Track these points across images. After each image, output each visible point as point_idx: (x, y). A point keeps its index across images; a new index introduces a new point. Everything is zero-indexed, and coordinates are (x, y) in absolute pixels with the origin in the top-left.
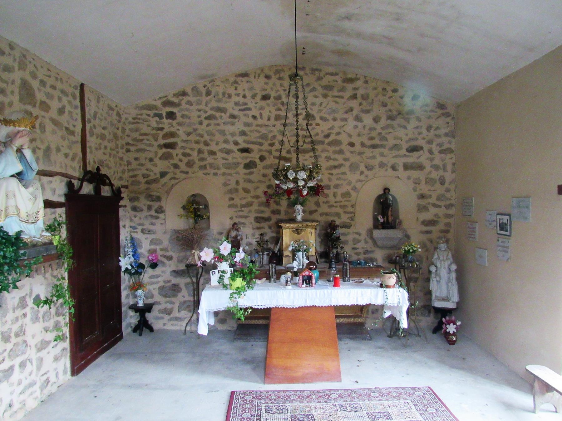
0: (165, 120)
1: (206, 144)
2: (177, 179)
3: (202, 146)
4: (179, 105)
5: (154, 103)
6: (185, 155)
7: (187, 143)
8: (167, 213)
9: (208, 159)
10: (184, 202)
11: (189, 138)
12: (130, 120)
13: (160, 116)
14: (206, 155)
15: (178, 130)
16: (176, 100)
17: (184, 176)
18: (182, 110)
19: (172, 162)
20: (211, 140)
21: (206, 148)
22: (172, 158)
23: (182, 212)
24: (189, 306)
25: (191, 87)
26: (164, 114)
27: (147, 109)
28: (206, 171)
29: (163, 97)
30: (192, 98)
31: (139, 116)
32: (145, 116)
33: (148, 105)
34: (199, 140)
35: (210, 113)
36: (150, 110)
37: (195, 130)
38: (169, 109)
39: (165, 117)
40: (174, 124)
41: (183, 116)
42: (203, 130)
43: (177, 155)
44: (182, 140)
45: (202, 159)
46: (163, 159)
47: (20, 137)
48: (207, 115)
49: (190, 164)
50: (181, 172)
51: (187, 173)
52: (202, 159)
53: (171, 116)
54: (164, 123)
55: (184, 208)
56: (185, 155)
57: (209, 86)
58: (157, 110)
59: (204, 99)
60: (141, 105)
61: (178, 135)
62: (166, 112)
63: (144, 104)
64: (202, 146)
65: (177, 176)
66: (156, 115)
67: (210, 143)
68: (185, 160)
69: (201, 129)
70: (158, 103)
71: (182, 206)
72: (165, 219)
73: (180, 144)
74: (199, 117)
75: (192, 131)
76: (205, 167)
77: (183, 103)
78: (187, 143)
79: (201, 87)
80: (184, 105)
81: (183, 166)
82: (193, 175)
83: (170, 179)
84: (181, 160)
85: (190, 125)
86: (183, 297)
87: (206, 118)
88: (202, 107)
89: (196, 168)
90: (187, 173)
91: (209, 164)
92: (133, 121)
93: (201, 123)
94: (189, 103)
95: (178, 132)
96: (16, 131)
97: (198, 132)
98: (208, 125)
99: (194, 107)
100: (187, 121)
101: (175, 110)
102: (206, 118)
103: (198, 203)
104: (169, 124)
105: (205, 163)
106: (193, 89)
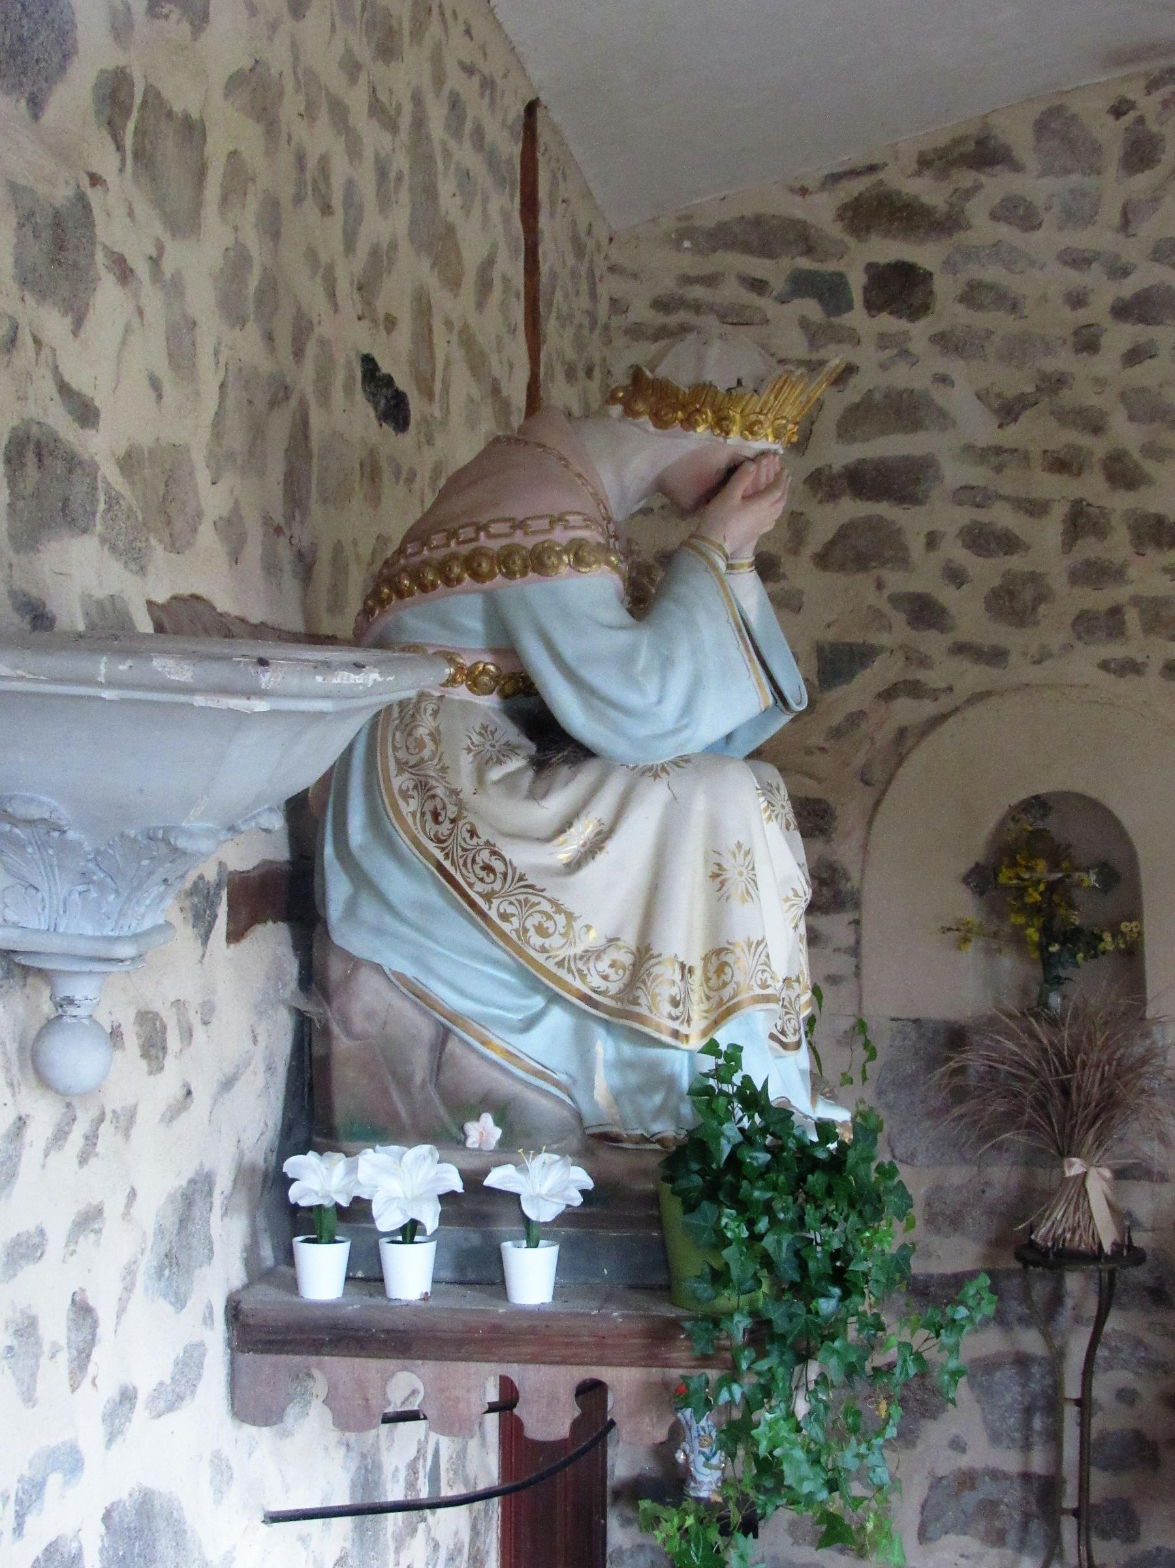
0: (857, 318)
1: (1121, 473)
2: (934, 694)
3: (1092, 487)
4: (946, 224)
5: (796, 208)
6: (982, 540)
7: (999, 469)
8: (870, 912)
9: (1132, 572)
10: (976, 849)
11: (1012, 435)
12: (641, 312)
13: (831, 292)
14: (1118, 546)
15: (943, 380)
16: (929, 192)
17: (973, 676)
18: (969, 254)
19: (897, 581)
20: (1153, 451)
21: (1120, 503)
22: (902, 561)
23: (965, 906)
24: (989, 1507)
25: (1038, 109)
26: (857, 281)
27: (746, 248)
28: (1116, 651)
29: (854, 173)
30: (1034, 185)
31: (698, 292)
32: (731, 292)
33: (758, 221)
34: (1075, 450)
35: (1148, 275)
36: (766, 250)
37: (1055, 383)
38: (887, 250)
39: (857, 296)
40: (919, 344)
41: (973, 295)
42: (1100, 383)
43: (932, 540)
44: (968, 448)
45: (1096, 574)
46: (842, 567)
47: (748, 498)
48: (1128, 288)
49: (1014, 602)
50: (960, 649)
51: (996, 656)
52: (1096, 574)
53: (899, 288)
54: (853, 338)
55: (981, 879)
56: (982, 540)
57: (1148, 105)
58: (809, 251)
59: (1115, 187)
60: (708, 222)
61: (942, 414)
62: (871, 267)
63: (729, 213)
64: (1092, 487)
65: (932, 678)
66: (802, 284)
67: (1149, 466)
68: (986, 572)
69: (1096, 379)
70: (821, 212)
71: (964, 867)
72: (855, 951)
73: (956, 473)
74: (1077, 300)
75: (1030, 389)
76: (1112, 623)
77: (977, 211)
78: (999, 469)
79: (1092, 113)
80: (983, 228)
81: (968, 612)
82: (1035, 674)
83: (889, 694)
84: (955, 576)
85: (1017, 349)
86: (957, 1445)
87: (1122, 311)
88: (1100, 237)
89: (1052, 630)
90: (996, 656)
91: (1136, 601)
92: (656, 319)
93: (1087, 342)
94: (1019, 213)
95: (939, 395)
96: (721, 460)
97: (1067, 397)
98: (1135, 356)
99: (1048, 239)
100: (1000, 322)
101: (924, 254)
102: (1122, 311)
103: (1057, 855)
104: (884, 341)
105: (1119, 594)
106: (1041, 127)
